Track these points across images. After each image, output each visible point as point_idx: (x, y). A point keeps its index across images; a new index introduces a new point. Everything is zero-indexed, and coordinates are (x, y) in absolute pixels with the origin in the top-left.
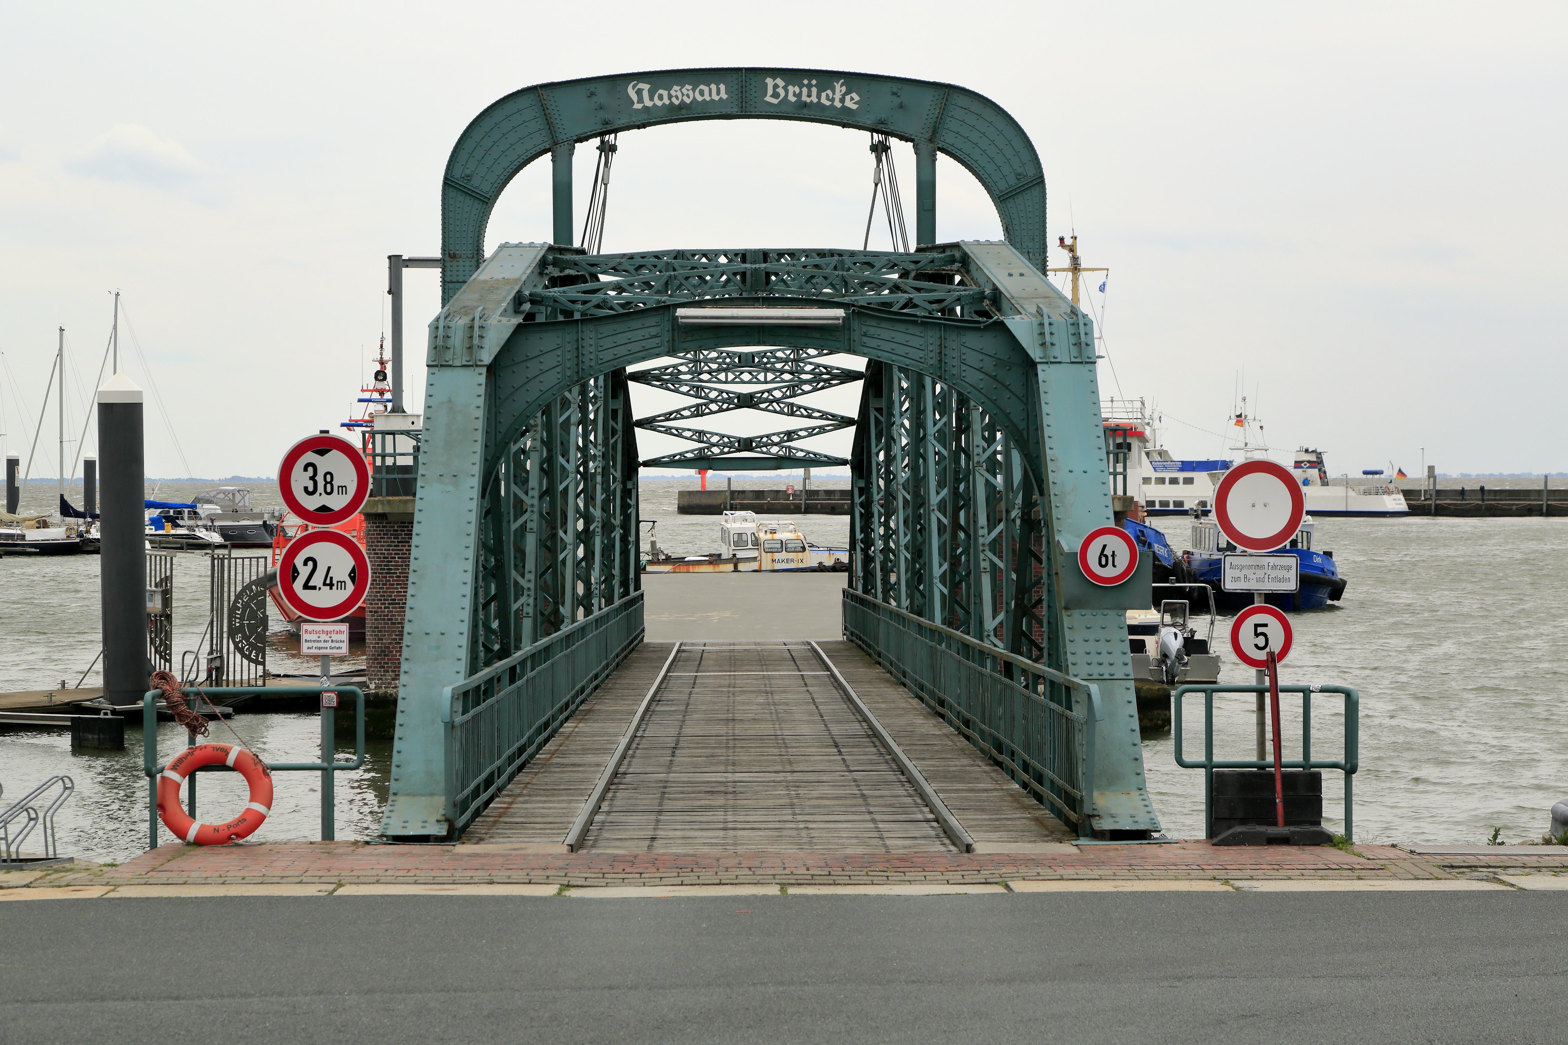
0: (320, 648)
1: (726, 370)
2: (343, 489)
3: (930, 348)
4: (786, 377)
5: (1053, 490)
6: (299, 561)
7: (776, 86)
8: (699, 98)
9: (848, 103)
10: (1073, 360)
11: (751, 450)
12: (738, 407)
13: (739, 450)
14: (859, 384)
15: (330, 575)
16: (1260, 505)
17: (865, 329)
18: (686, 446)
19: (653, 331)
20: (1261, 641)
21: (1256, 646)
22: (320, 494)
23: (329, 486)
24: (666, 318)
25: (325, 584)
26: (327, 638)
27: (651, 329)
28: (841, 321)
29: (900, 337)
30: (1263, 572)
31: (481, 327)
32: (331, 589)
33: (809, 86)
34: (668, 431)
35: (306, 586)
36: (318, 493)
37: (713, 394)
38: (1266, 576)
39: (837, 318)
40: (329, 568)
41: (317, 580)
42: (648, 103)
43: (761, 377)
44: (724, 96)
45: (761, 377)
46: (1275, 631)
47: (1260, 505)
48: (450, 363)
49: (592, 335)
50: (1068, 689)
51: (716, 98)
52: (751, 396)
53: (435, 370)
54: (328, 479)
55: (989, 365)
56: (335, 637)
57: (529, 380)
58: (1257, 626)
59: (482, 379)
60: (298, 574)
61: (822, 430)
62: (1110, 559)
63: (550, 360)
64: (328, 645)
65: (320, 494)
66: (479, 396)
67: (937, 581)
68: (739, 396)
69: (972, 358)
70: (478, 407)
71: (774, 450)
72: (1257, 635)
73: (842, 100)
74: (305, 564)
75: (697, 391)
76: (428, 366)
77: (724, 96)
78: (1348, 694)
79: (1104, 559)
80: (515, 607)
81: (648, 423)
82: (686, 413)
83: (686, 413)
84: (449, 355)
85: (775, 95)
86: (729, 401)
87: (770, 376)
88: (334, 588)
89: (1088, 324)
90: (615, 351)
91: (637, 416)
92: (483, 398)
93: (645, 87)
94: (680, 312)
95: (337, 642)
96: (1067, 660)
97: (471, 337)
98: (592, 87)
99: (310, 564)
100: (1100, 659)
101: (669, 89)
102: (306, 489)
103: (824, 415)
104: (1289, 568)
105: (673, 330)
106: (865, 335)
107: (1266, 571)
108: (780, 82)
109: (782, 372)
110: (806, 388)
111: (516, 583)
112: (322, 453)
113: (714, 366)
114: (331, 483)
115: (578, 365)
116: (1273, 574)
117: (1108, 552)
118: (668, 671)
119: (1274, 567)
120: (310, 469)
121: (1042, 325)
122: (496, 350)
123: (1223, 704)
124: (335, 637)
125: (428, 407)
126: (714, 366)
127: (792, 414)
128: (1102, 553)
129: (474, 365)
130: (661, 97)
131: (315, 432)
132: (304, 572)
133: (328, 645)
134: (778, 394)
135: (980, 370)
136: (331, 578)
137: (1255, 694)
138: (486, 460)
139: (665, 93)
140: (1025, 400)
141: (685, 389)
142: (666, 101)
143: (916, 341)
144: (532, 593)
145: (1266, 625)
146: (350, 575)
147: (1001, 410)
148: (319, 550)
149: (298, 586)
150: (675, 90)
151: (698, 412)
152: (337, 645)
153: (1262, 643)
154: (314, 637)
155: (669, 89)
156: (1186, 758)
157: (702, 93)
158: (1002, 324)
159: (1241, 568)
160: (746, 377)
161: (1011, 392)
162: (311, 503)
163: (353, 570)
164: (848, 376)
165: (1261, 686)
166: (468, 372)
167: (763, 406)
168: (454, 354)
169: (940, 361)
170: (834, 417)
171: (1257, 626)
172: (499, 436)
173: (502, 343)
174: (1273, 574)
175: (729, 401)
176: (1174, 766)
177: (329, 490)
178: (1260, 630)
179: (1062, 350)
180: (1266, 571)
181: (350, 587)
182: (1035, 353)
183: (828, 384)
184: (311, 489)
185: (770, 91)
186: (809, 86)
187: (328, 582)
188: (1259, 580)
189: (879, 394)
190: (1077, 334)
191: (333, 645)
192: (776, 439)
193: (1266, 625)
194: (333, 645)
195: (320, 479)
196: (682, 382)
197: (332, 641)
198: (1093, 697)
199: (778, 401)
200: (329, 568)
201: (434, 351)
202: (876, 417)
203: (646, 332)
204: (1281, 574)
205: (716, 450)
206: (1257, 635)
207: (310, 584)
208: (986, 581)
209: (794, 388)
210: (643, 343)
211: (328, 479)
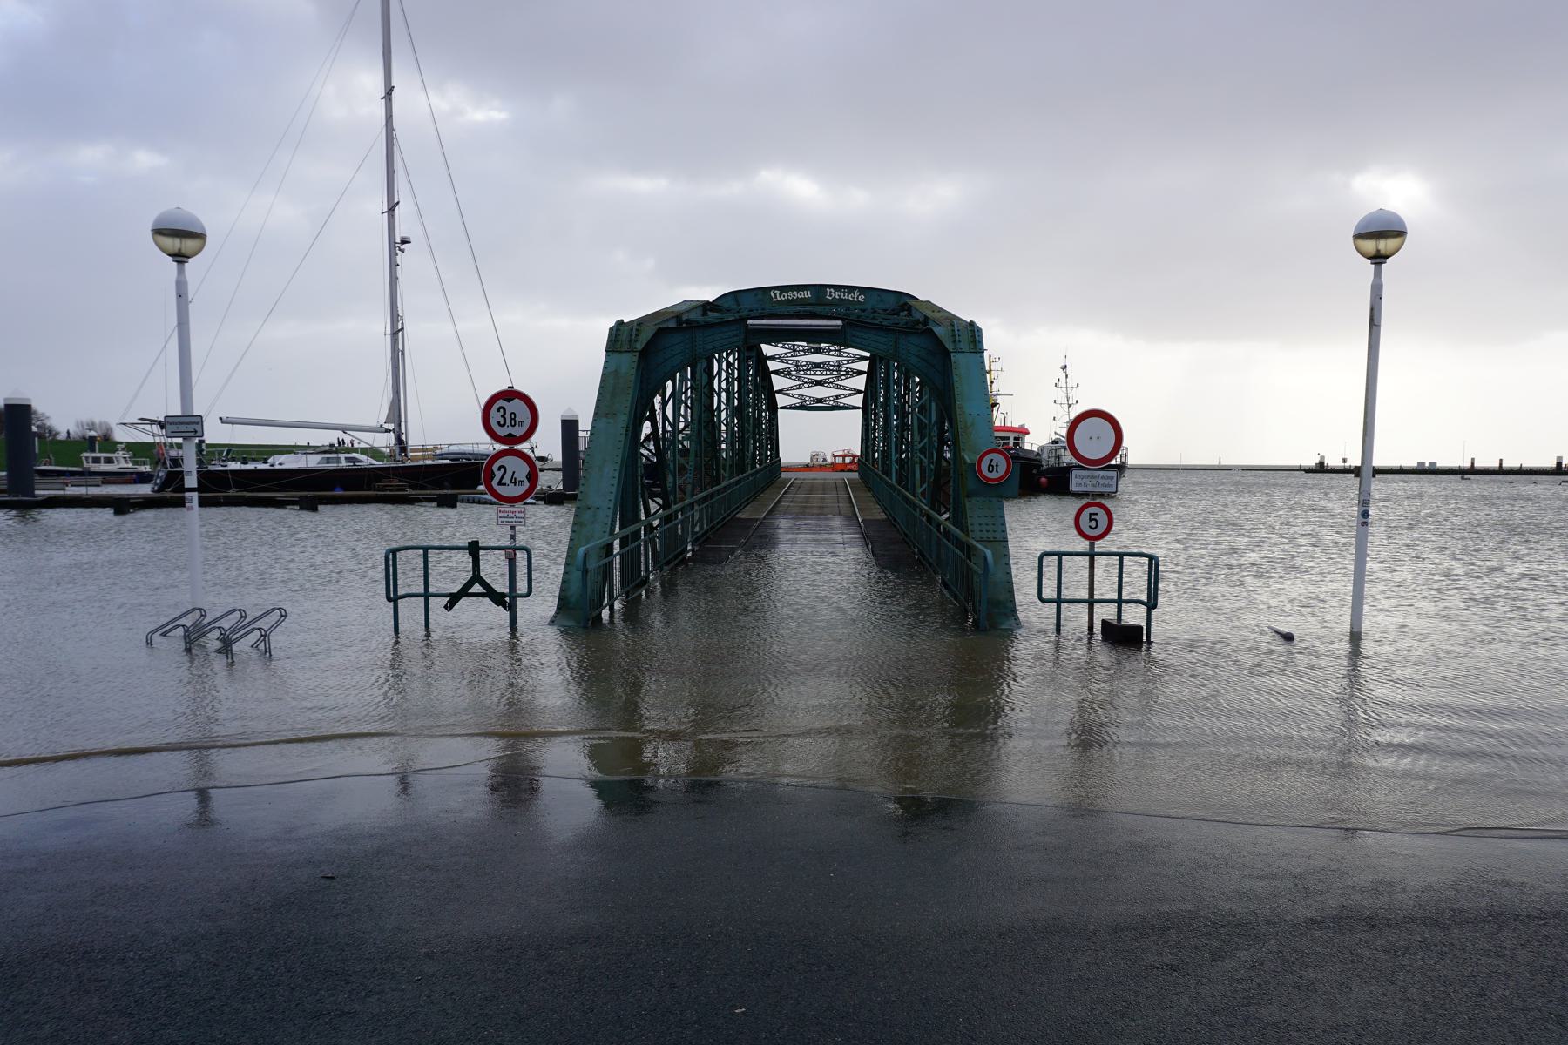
1: (810, 370)
2: (522, 423)
4: (835, 373)
5: (960, 425)
6: (495, 467)
7: (831, 292)
9: (860, 299)
11: (822, 403)
12: (816, 385)
13: (817, 403)
16: (1094, 438)
17: (854, 332)
18: (797, 401)
19: (735, 333)
21: (1090, 527)
25: (511, 482)
31: (637, 330)
33: (844, 292)
34: (788, 395)
35: (500, 483)
37: (805, 380)
39: (838, 326)
40: (514, 472)
41: (507, 480)
42: (779, 299)
43: (824, 373)
45: (824, 373)
47: (1094, 438)
50: (968, 546)
52: (821, 381)
56: (518, 515)
58: (1091, 514)
59: (636, 359)
61: (850, 395)
64: (514, 519)
67: (894, 463)
68: (816, 381)
71: (831, 403)
73: (858, 298)
74: (499, 469)
75: (799, 379)
78: (1151, 558)
79: (991, 467)
81: (780, 392)
84: (618, 345)
85: (830, 296)
87: (828, 373)
89: (980, 330)
93: (778, 292)
94: (750, 322)
96: (967, 523)
99: (502, 469)
100: (988, 528)
102: (499, 423)
103: (851, 389)
104: (1112, 478)
106: (854, 336)
109: (833, 371)
110: (843, 377)
112: (509, 400)
113: (805, 368)
114: (514, 419)
116: (1102, 481)
117: (994, 463)
118: (785, 493)
119: (1103, 477)
120: (502, 410)
121: (953, 331)
122: (645, 342)
123: (1070, 564)
124: (518, 515)
126: (805, 368)
127: (838, 388)
128: (990, 464)
129: (631, 351)
132: (498, 474)
133: (514, 519)
134: (832, 380)
135: (917, 356)
136: (515, 479)
141: (794, 378)
144: (692, 472)
145: (1097, 514)
148: (510, 462)
149: (495, 483)
153: (1094, 526)
158: (932, 330)
160: (818, 373)
162: (502, 432)
163: (529, 474)
164: (860, 373)
166: (629, 355)
170: (855, 390)
171: (1091, 514)
173: (649, 338)
174: (1102, 481)
176: (1037, 599)
178: (1093, 517)
179: (964, 346)
182: (950, 347)
183: (852, 376)
184: (502, 423)
186: (844, 292)
188: (1093, 486)
189: (872, 380)
190: (974, 336)
192: (831, 399)
193: (1097, 514)
195: (507, 416)
196: (793, 375)
198: (988, 558)
199: (831, 383)
200: (514, 472)
204: (1107, 482)
205: (808, 403)
206: (1091, 520)
208: (917, 467)
209: (838, 378)
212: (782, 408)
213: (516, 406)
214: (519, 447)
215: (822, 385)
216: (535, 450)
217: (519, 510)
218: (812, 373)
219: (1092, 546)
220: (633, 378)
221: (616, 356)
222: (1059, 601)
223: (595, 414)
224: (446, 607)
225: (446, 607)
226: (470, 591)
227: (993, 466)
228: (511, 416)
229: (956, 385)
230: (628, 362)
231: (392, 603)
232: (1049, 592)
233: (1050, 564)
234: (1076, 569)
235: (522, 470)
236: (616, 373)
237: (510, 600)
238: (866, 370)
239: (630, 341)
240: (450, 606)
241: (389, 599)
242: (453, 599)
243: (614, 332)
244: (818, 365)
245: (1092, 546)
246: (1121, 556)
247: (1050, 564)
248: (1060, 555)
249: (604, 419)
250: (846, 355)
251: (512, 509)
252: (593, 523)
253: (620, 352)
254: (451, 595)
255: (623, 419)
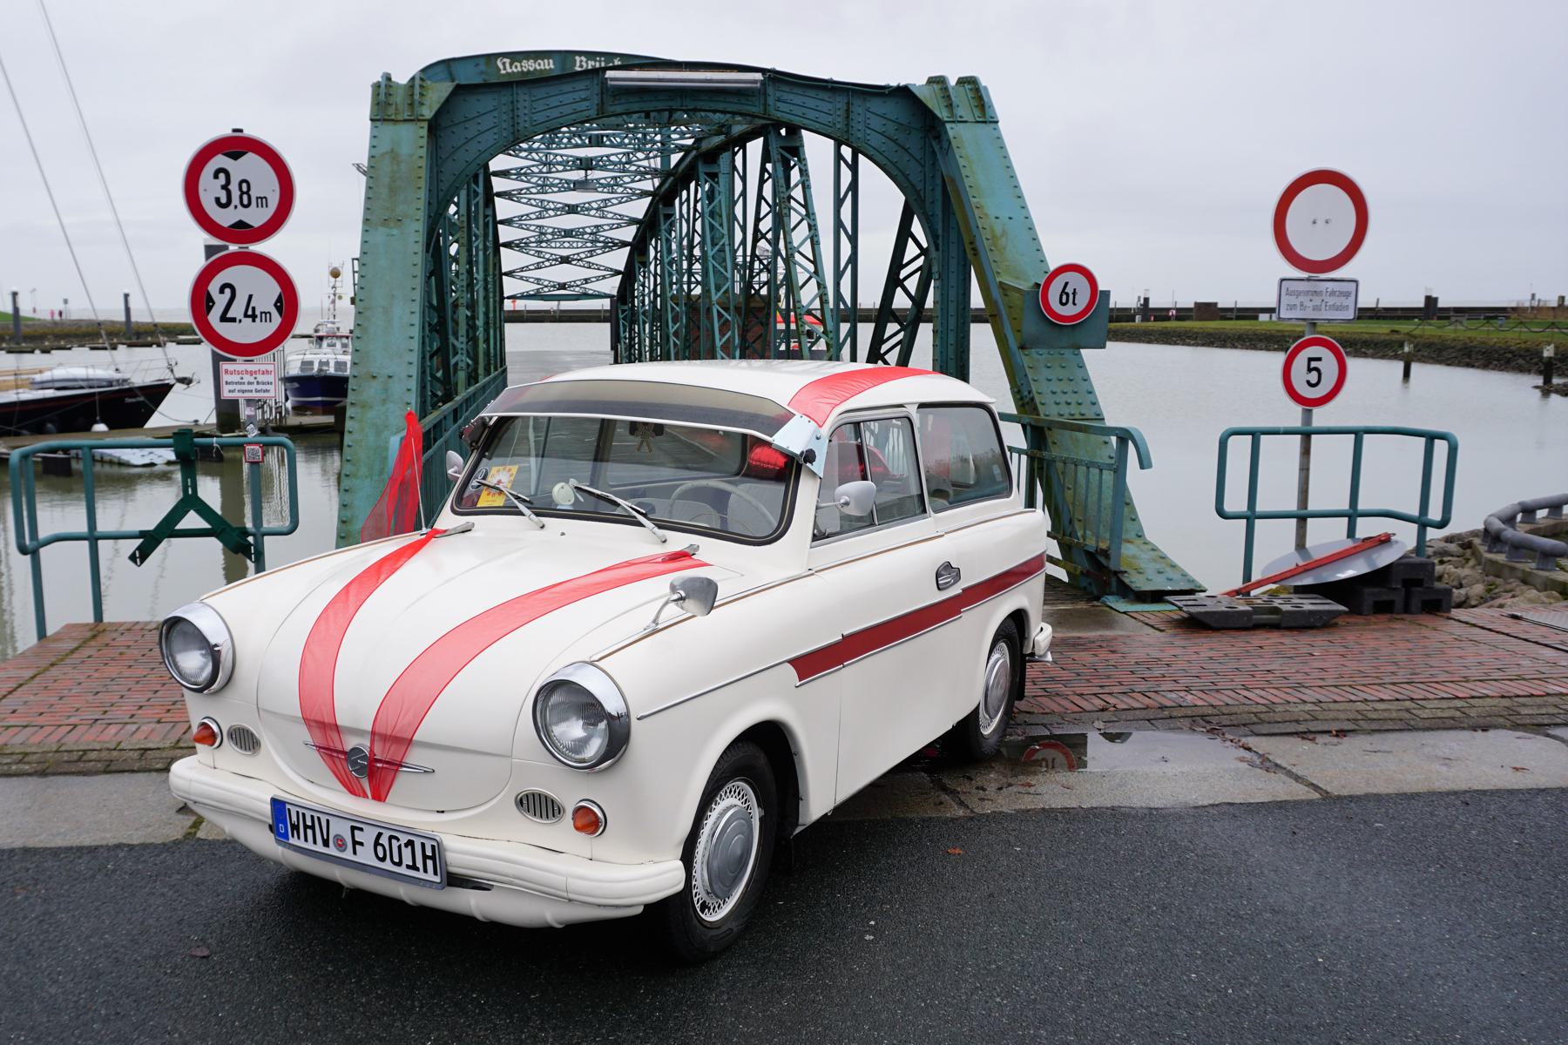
0: (243, 391)
2: (263, 200)
3: (838, 113)
6: (213, 288)
7: (581, 61)
8: (538, 68)
10: (978, 119)
11: (565, 289)
12: (561, 263)
13: (558, 289)
14: (628, 249)
15: (252, 305)
16: (1320, 222)
18: (530, 287)
19: (583, 95)
20: (1313, 377)
21: (1308, 382)
22: (236, 207)
23: (245, 197)
24: (595, 82)
25: (246, 315)
26: (251, 379)
27: (581, 93)
28: (759, 85)
29: (811, 103)
30: (1321, 298)
32: (254, 321)
34: (521, 278)
36: (232, 206)
37: (547, 256)
38: (1324, 304)
39: (755, 82)
40: (250, 297)
41: (237, 310)
42: (509, 70)
44: (552, 66)
46: (1329, 365)
48: (393, 117)
49: (526, 97)
51: (547, 67)
52: (568, 257)
53: (378, 124)
54: (245, 189)
55: (891, 129)
56: (261, 378)
57: (468, 141)
59: (424, 132)
60: (214, 303)
61: (604, 277)
62: (1071, 297)
63: (488, 122)
64: (250, 387)
65: (236, 207)
66: (422, 147)
68: (561, 257)
69: (876, 122)
70: (421, 157)
71: (577, 289)
72: (1310, 370)
74: (222, 291)
76: (372, 120)
77: (552, 66)
79: (1066, 296)
80: (453, 361)
82: (531, 267)
83: (531, 267)
84: (391, 111)
85: (581, 66)
86: (556, 260)
88: (258, 320)
90: (548, 113)
91: (504, 270)
92: (425, 149)
93: (507, 61)
94: (609, 74)
95: (263, 383)
97: (412, 95)
98: (477, 61)
99: (228, 291)
101: (520, 62)
102: (218, 200)
103: (607, 269)
105: (602, 93)
106: (779, 100)
107: (1324, 297)
108: (584, 59)
111: (453, 345)
112: (235, 156)
114: (247, 193)
115: (513, 126)
116: (1331, 301)
117: (1069, 290)
119: (1333, 293)
120: (222, 176)
122: (436, 107)
124: (261, 378)
125: (372, 157)
127: (590, 268)
130: (516, 67)
131: (226, 131)
132: (221, 301)
134: (583, 256)
136: (254, 309)
137: (1299, 436)
138: (429, 216)
139: (518, 64)
140: (922, 162)
141: (532, 252)
142: (519, 69)
143: (825, 107)
145: (1319, 359)
146: (275, 305)
147: (900, 171)
149: (214, 318)
150: (524, 63)
151: (538, 267)
152: (264, 387)
153: (1314, 381)
154: (236, 378)
155: (520, 62)
156: (1228, 507)
157: (539, 65)
159: (1298, 294)
161: (910, 154)
162: (225, 218)
163: (279, 299)
164: (624, 244)
165: (1307, 428)
167: (574, 262)
168: (396, 109)
169: (847, 125)
170: (612, 270)
171: (1310, 360)
172: (441, 194)
173: (442, 100)
174: (1331, 301)
175: (556, 260)
177: (245, 202)
178: (1313, 364)
179: (963, 111)
180: (1324, 297)
181: (277, 319)
182: (942, 113)
184: (224, 200)
185: (578, 64)
187: (250, 313)
188: (1316, 308)
190: (980, 98)
191: (260, 387)
193: (1319, 359)
194: (260, 387)
195: (234, 187)
197: (258, 383)
199: (581, 260)
200: (250, 297)
201: (376, 107)
202: (710, 223)
203: (577, 96)
205: (546, 289)
206: (1310, 370)
207: (229, 315)
209: (592, 253)
210: (574, 106)
211: (245, 189)
212: (508, 298)
213: (250, 167)
214: (259, 248)
215: (569, 263)
216: (175, 369)
217: (263, 368)
218: (558, 245)
219: (1307, 416)
220: (423, 163)
221: (388, 130)
222: (1251, 517)
223: (366, 221)
224: (133, 558)
225: (133, 558)
226: (178, 527)
227: (1067, 294)
228: (240, 188)
229: (964, 172)
230: (411, 140)
231: (28, 557)
232: (1236, 501)
233: (1240, 448)
234: (1280, 455)
235: (266, 291)
236: (393, 155)
237: (255, 540)
238: (622, 268)
239: (411, 105)
240: (141, 556)
241: (23, 550)
242: (148, 543)
243: (383, 90)
244: (568, 233)
245: (1307, 416)
246: (1359, 434)
247: (1240, 448)
248: (1255, 434)
249: (381, 229)
250: (610, 215)
251: (250, 367)
252: (384, 401)
253: (395, 121)
254: (142, 534)
255: (415, 231)
